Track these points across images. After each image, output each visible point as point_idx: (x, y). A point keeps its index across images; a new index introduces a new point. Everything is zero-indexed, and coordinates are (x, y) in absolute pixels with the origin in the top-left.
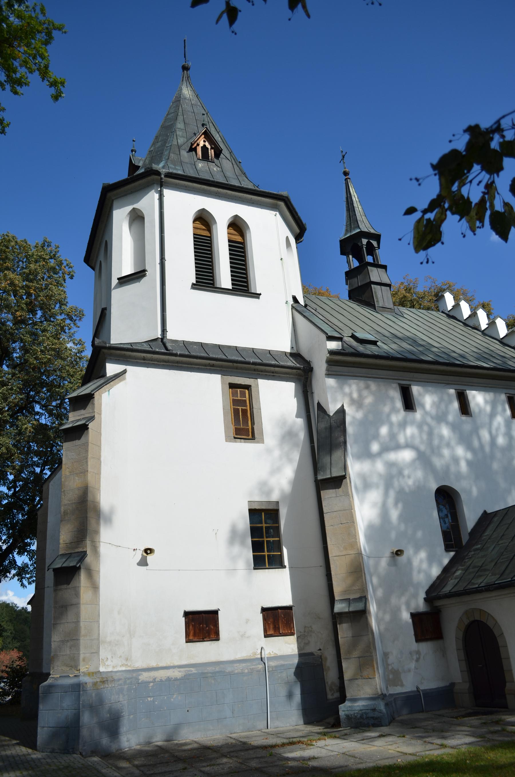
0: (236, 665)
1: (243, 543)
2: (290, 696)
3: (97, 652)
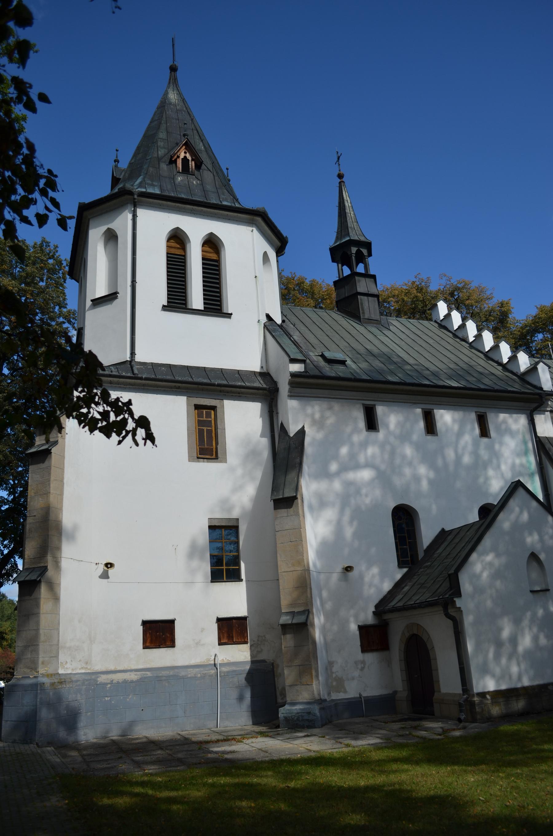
0: (189, 670)
1: (202, 558)
2: (241, 698)
3: (57, 656)
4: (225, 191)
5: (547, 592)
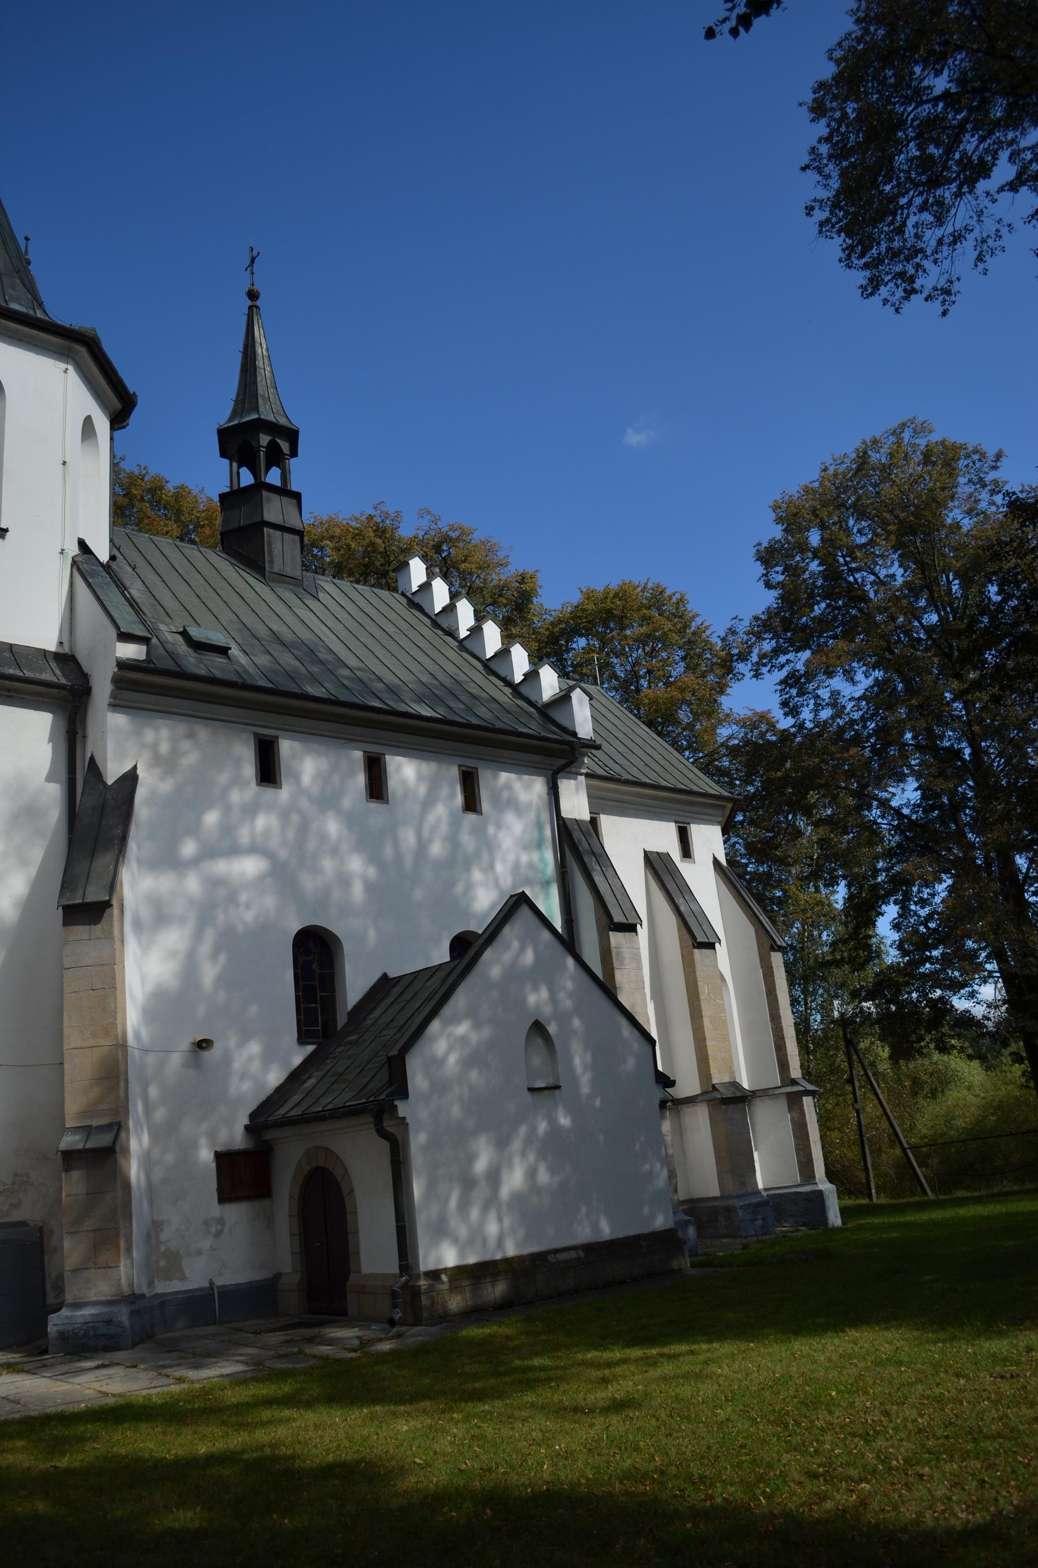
4: (19, 282)
5: (557, 1091)
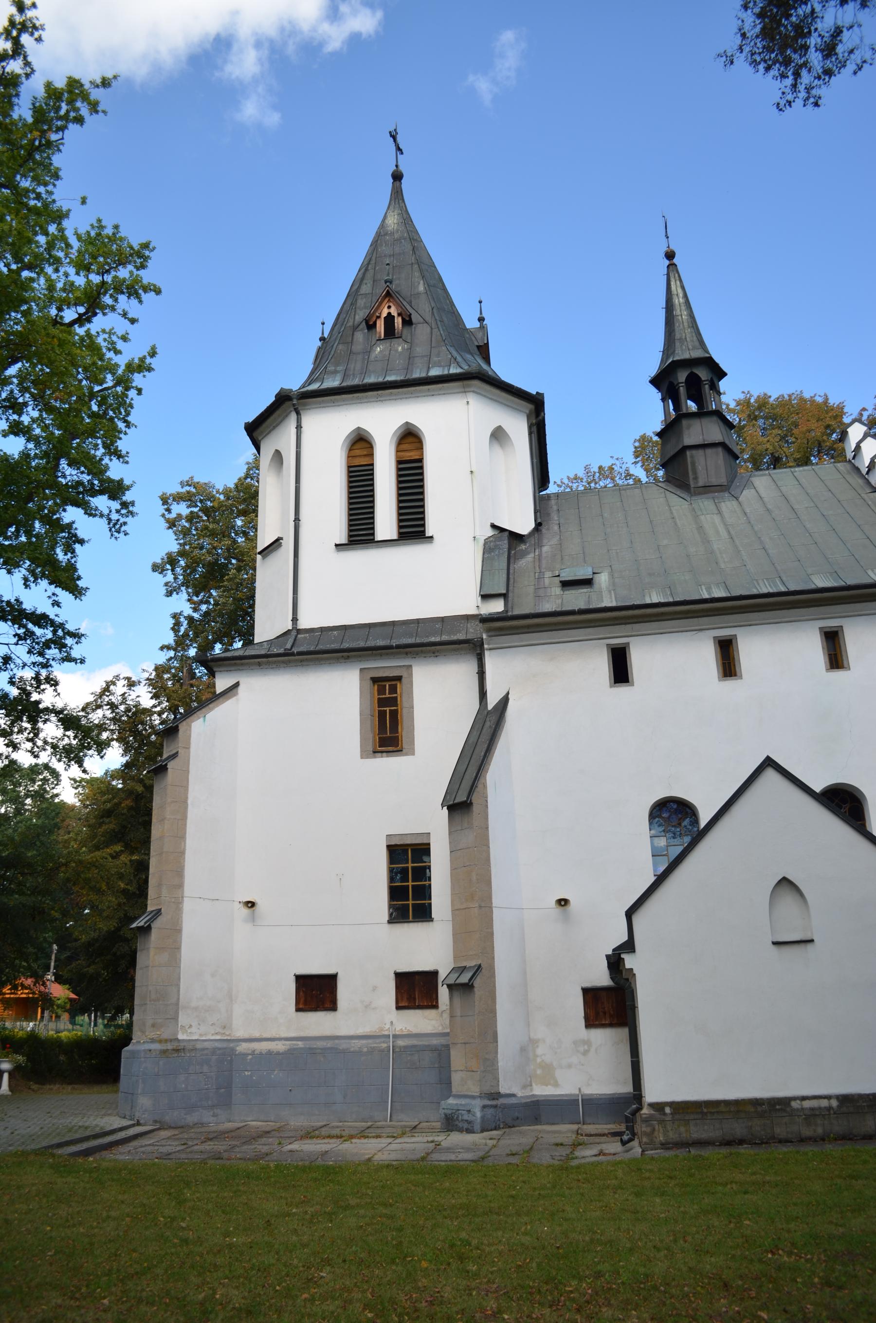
3: (176, 1018)
5: (809, 946)
